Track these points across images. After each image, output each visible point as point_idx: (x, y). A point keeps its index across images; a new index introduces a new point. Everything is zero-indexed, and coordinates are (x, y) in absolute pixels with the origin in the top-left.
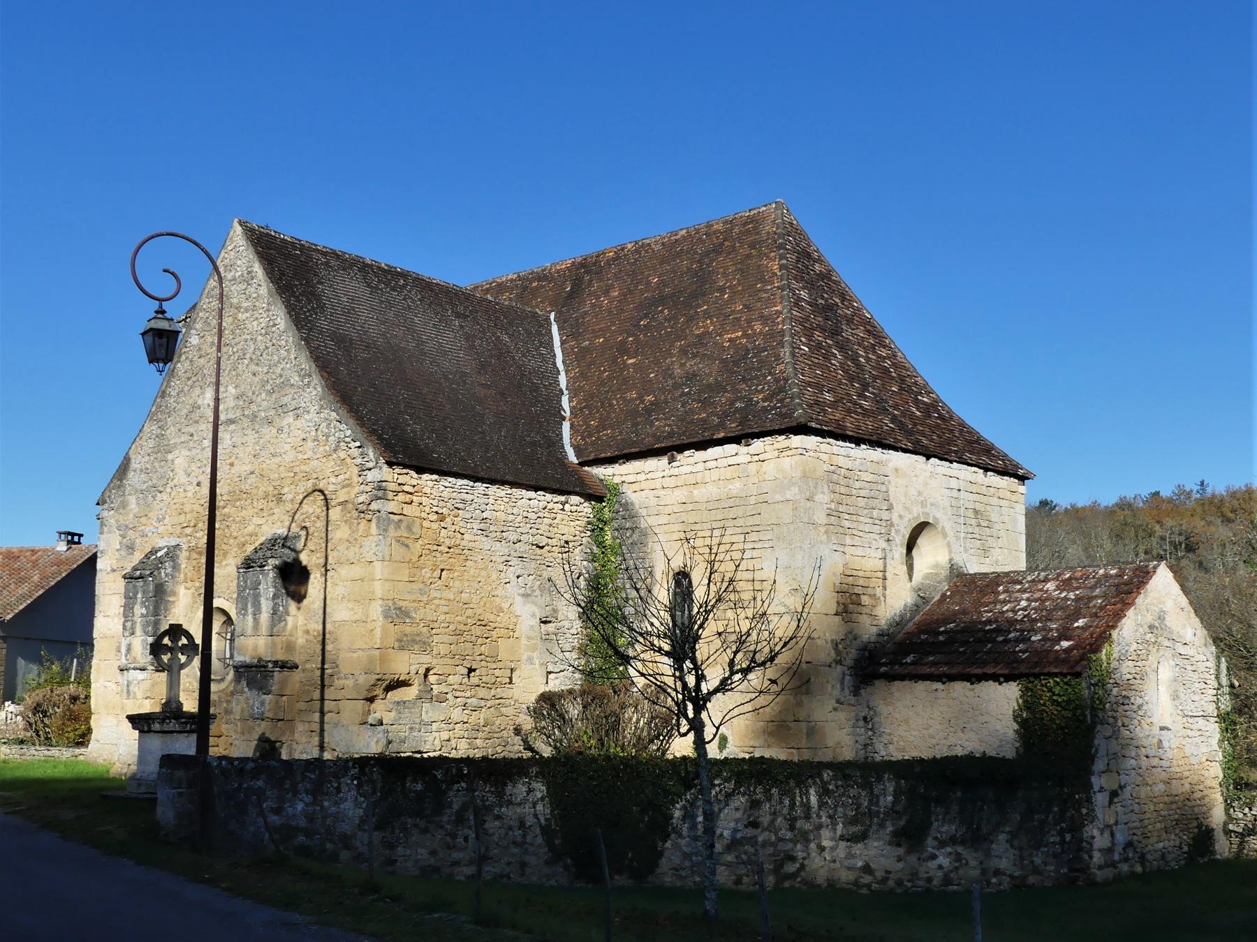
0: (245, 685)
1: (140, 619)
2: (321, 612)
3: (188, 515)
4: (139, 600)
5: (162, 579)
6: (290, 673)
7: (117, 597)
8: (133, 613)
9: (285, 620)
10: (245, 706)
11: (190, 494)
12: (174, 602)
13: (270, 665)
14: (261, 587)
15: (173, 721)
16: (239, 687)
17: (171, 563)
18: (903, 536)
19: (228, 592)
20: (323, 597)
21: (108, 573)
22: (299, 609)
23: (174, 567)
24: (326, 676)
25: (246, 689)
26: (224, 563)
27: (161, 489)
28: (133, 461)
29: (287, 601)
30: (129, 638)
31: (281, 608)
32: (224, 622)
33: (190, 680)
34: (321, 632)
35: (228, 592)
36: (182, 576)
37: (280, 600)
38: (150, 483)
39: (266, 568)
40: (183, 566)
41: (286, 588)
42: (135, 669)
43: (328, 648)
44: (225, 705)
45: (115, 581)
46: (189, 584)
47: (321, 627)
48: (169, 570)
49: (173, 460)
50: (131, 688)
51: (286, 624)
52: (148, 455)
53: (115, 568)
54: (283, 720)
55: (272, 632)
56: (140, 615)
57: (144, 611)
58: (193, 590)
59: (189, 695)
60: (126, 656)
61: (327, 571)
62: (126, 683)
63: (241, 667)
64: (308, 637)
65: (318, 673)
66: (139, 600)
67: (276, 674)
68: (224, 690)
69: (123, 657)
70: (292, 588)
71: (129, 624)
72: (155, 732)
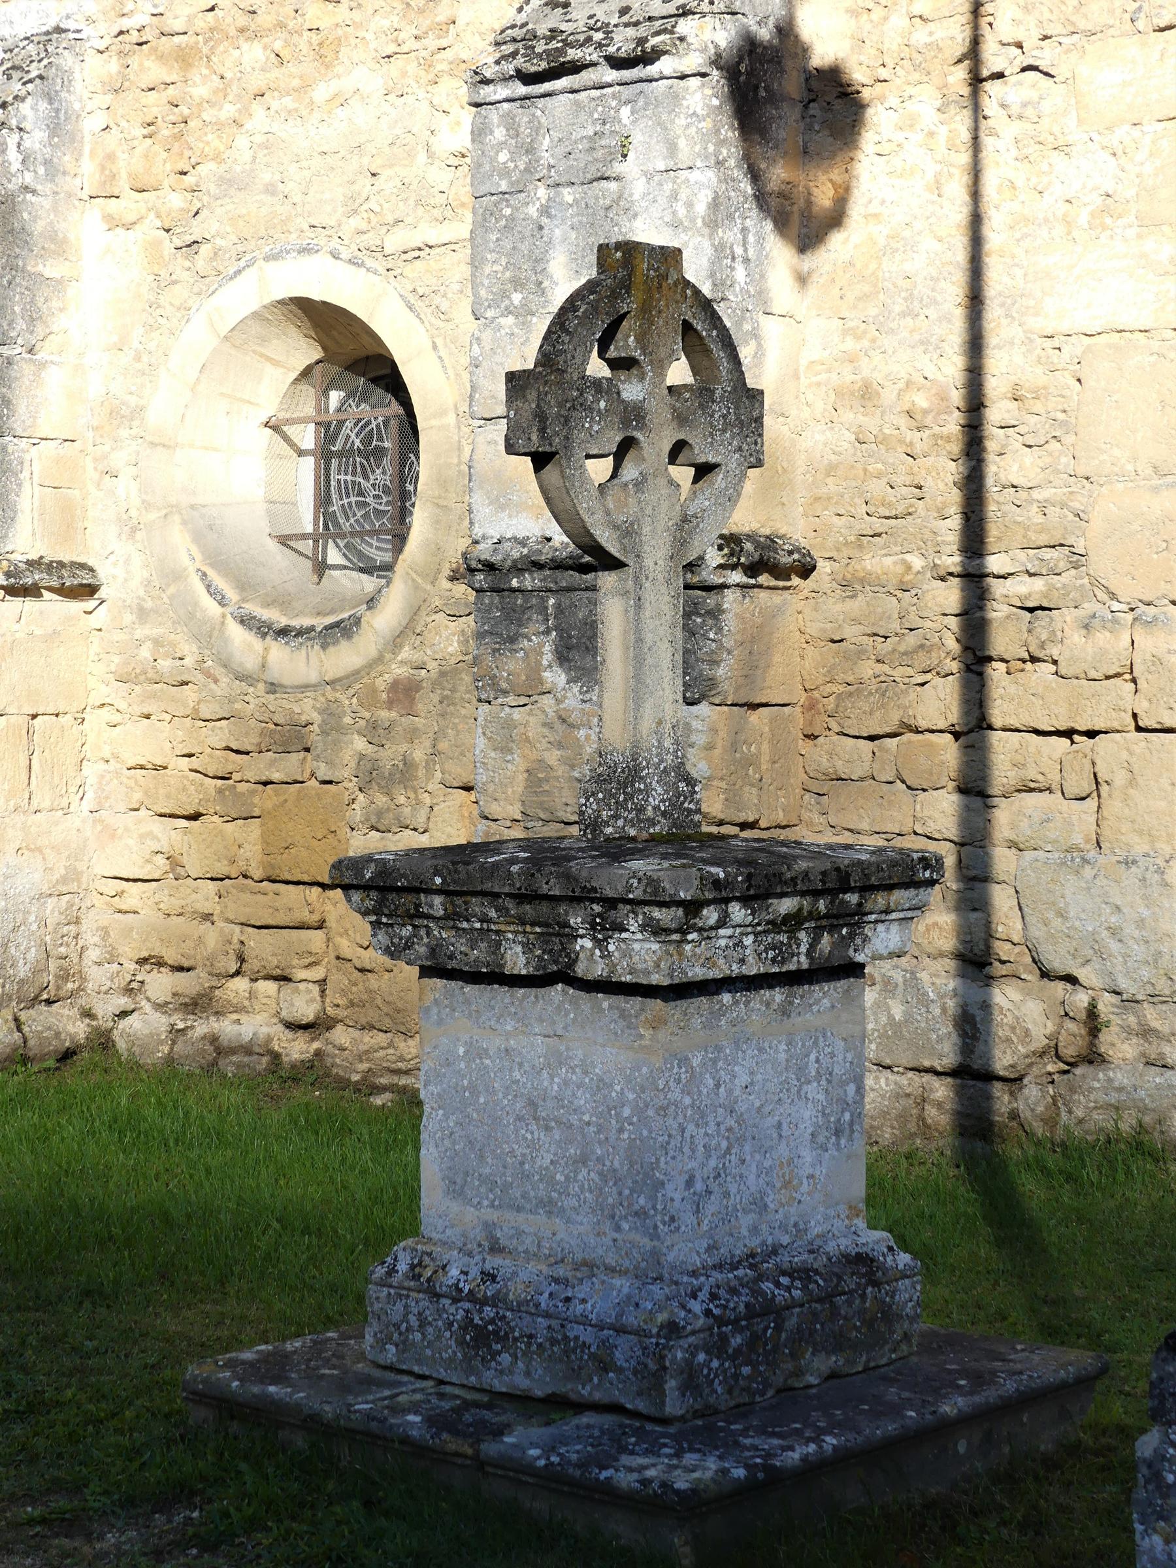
0: (547, 657)
2: (954, 291)
5: (9, 177)
6: (777, 598)
10: (553, 757)
12: (59, 285)
14: (629, 168)
15: (738, 912)
16: (512, 665)
17: (43, 105)
18: (847, 240)
19: (356, 222)
20: (959, 213)
22: (802, 280)
23: (55, 127)
24: (997, 612)
26: (321, 93)
29: (761, 239)
32: (306, 373)
33: (156, 632)
34: (957, 397)
35: (356, 222)
39: (664, 65)
40: (91, 125)
41: (755, 176)
43: (997, 470)
44: (360, 744)
46: (129, 205)
47: (953, 368)
48: (36, 139)
58: (149, 229)
59: (154, 696)
61: (976, 80)
64: (871, 423)
65: (950, 596)
67: (730, 599)
68: (355, 674)
70: (778, 174)
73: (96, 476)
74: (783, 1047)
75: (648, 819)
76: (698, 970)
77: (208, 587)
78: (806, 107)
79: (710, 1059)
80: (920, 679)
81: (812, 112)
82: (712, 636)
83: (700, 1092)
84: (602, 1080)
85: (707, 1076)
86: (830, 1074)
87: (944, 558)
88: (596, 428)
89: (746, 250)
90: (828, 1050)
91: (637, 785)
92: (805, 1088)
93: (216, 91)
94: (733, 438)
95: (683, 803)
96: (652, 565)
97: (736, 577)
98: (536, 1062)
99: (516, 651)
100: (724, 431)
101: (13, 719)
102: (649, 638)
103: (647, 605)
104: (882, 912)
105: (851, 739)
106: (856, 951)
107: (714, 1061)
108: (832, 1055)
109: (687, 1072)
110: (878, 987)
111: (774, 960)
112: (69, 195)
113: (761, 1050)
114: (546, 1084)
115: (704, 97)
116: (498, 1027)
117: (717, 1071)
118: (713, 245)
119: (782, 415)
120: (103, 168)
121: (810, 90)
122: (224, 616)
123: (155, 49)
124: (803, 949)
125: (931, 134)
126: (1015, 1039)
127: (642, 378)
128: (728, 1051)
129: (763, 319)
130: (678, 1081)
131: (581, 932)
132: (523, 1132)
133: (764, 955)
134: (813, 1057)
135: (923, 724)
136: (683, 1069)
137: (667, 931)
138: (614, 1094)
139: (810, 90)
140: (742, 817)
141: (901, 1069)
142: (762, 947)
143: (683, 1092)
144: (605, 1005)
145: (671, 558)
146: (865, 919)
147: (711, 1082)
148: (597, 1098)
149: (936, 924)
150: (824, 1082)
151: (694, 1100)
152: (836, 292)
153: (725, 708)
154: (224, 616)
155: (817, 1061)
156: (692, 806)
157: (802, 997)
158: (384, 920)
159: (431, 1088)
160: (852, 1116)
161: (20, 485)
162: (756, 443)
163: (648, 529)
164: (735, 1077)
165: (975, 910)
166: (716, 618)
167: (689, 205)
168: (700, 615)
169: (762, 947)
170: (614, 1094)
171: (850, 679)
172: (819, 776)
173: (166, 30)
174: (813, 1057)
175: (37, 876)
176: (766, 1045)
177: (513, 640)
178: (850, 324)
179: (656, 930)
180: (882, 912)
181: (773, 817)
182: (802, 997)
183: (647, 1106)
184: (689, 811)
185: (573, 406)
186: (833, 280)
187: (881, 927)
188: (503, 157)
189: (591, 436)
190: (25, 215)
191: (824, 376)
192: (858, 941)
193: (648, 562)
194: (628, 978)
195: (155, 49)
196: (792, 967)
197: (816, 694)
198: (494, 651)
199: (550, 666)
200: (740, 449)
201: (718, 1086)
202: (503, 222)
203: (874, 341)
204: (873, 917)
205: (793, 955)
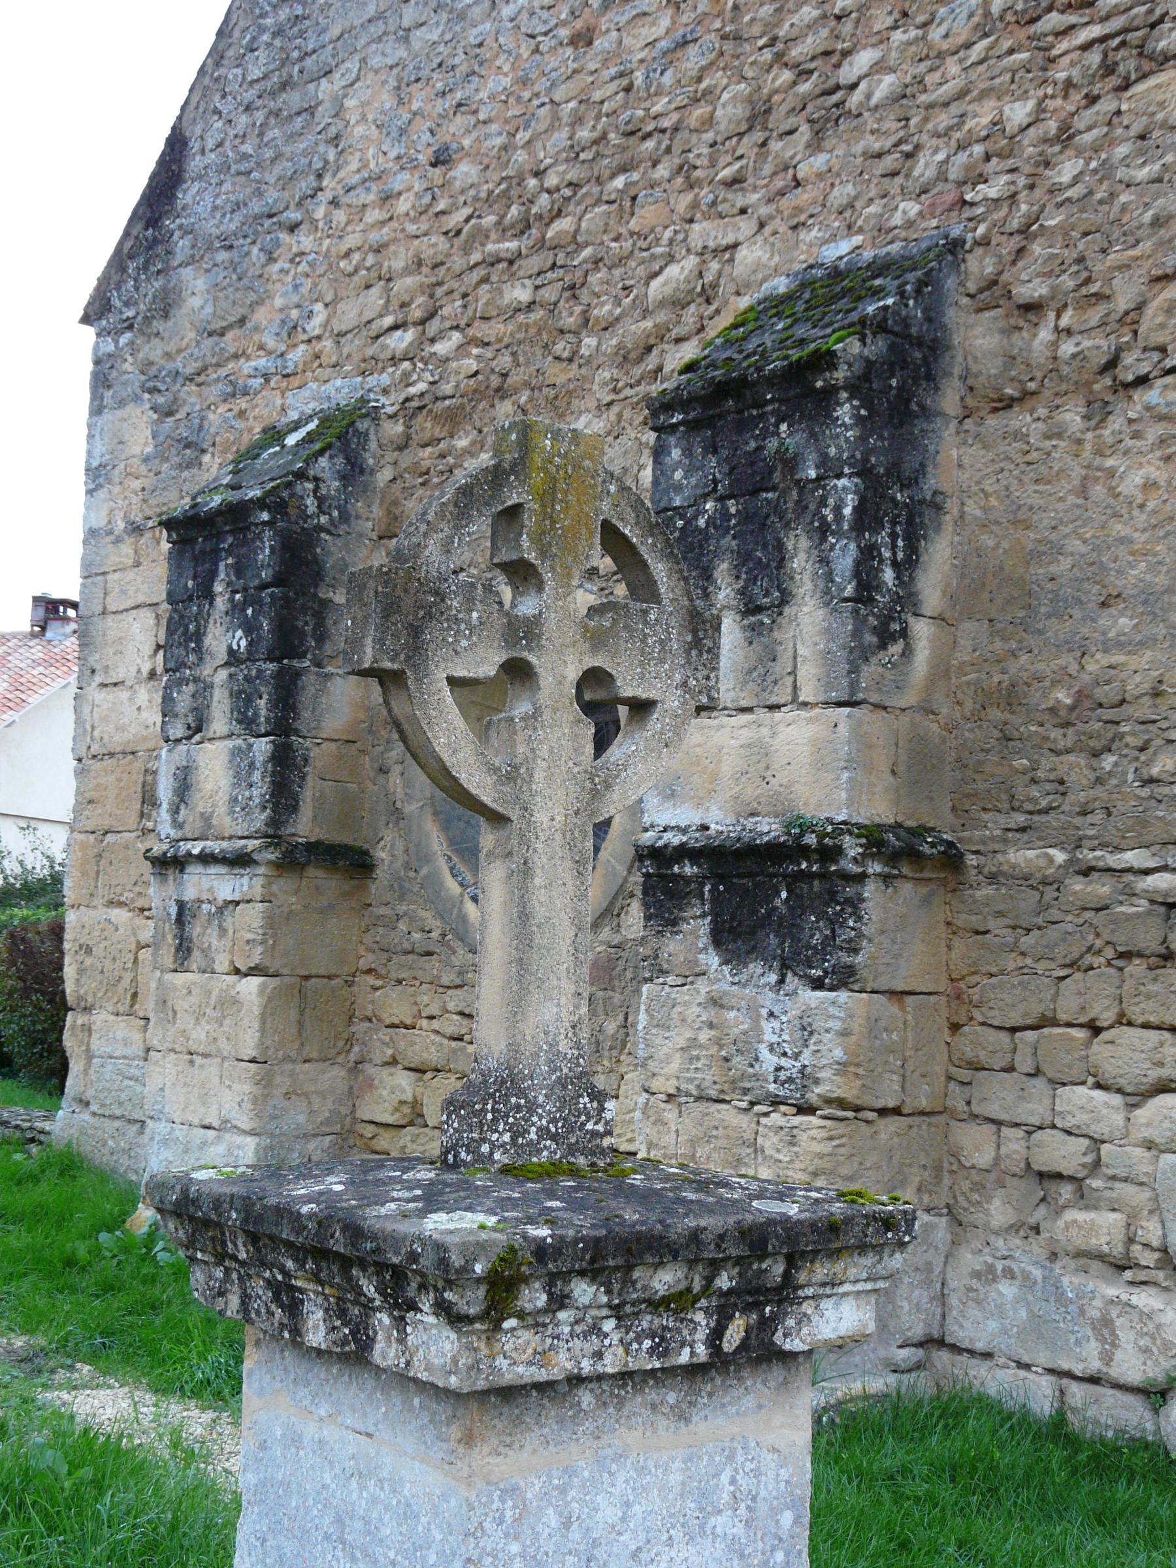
0: (703, 940)
1: (223, 674)
3: (398, 286)
4: (221, 603)
7: (147, 618)
8: (199, 650)
9: (904, 633)
11: (403, 205)
13: (852, 847)
15: (583, 1291)
21: (118, 541)
25: (712, 960)
27: (294, 215)
28: (195, 145)
30: (182, 748)
31: (888, 575)
36: (377, 511)
37: (883, 537)
38: (256, 207)
42: (206, 859)
45: (137, 564)
49: (109, 1559)
50: (195, 930)
51: (907, 653)
52: (248, 108)
53: (138, 519)
54: (897, 1111)
55: (854, 686)
56: (222, 656)
57: (240, 641)
60: (175, 811)
62: (173, 910)
63: (683, 852)
66: (221, 603)
69: (164, 814)
71: (184, 699)
72: (404, 1380)
73: (372, 774)
74: (678, 1464)
75: (530, 1143)
76: (520, 1369)
77: (452, 869)
78: (960, 422)
79: (557, 1487)
80: (1062, 973)
81: (966, 427)
82: (851, 923)
83: (536, 1535)
84: (409, 1505)
85: (551, 1511)
86: (754, 1499)
87: (1085, 851)
88: (464, 643)
89: (894, 554)
90: (749, 1466)
91: (513, 1100)
92: (712, 1521)
93: (473, 443)
94: (672, 669)
95: (584, 1124)
96: (546, 820)
97: (875, 867)
98: (347, 1465)
99: (677, 933)
100: (662, 661)
101: (286, 980)
102: (540, 913)
103: (538, 871)
104: (824, 1285)
105: (992, 1030)
106: (785, 1335)
107: (563, 1490)
108: (757, 1473)
109: (515, 1507)
110: (1017, 1283)
111: (651, 1351)
112: (361, 535)
113: (641, 1471)
114: (355, 1496)
115: (853, 407)
116: (313, 1409)
117: (567, 1504)
118: (858, 546)
119: (933, 713)
120: (389, 512)
121: (965, 407)
122: (462, 895)
123: (431, 411)
124: (701, 1334)
125: (1079, 442)
126: (1155, 1350)
127: (540, 588)
128: (586, 1474)
129: (911, 620)
130: (501, 1521)
131: (377, 1303)
132: (329, 1557)
133: (635, 1346)
134: (725, 1478)
135: (1063, 1017)
136: (510, 1503)
137: (469, 1320)
138: (420, 1529)
139: (965, 407)
140: (880, 1104)
141: (1039, 1370)
142: (632, 1335)
143: (507, 1535)
144: (417, 1401)
145: (577, 813)
146: (800, 1293)
147: (553, 1520)
148: (403, 1529)
149: (1075, 1221)
150: (742, 1510)
151: (524, 1546)
152: (986, 596)
153: (864, 995)
154: (462, 895)
155: (733, 1481)
156: (600, 1128)
157: (710, 1395)
158: (199, 1255)
159: (249, 1475)
160: (787, 1554)
161: (303, 778)
162: (708, 678)
163: (543, 774)
164: (596, 1510)
165: (1114, 1210)
166: (855, 907)
167: (838, 509)
168: (838, 903)
169: (632, 1335)
170: (420, 1529)
171: (994, 970)
172: (963, 1064)
173: (440, 394)
174: (725, 1478)
175: (301, 1118)
176: (651, 1464)
177: (674, 923)
178: (999, 626)
179: (454, 1318)
180: (824, 1285)
181: (916, 1104)
182: (710, 1395)
183: (454, 1555)
184: (595, 1134)
185: (430, 614)
186: (984, 584)
187: (826, 1304)
188: (678, 475)
189: (457, 653)
190: (318, 550)
191: (973, 676)
192: (790, 1322)
193: (541, 817)
194: (424, 1376)
195: (431, 411)
196: (684, 1358)
197: (962, 985)
198: (659, 932)
199: (705, 949)
200: (685, 684)
201: (567, 1524)
202: (677, 534)
203: (1020, 641)
204: (809, 1291)
205: (683, 1344)
